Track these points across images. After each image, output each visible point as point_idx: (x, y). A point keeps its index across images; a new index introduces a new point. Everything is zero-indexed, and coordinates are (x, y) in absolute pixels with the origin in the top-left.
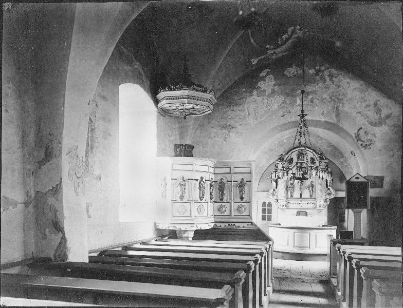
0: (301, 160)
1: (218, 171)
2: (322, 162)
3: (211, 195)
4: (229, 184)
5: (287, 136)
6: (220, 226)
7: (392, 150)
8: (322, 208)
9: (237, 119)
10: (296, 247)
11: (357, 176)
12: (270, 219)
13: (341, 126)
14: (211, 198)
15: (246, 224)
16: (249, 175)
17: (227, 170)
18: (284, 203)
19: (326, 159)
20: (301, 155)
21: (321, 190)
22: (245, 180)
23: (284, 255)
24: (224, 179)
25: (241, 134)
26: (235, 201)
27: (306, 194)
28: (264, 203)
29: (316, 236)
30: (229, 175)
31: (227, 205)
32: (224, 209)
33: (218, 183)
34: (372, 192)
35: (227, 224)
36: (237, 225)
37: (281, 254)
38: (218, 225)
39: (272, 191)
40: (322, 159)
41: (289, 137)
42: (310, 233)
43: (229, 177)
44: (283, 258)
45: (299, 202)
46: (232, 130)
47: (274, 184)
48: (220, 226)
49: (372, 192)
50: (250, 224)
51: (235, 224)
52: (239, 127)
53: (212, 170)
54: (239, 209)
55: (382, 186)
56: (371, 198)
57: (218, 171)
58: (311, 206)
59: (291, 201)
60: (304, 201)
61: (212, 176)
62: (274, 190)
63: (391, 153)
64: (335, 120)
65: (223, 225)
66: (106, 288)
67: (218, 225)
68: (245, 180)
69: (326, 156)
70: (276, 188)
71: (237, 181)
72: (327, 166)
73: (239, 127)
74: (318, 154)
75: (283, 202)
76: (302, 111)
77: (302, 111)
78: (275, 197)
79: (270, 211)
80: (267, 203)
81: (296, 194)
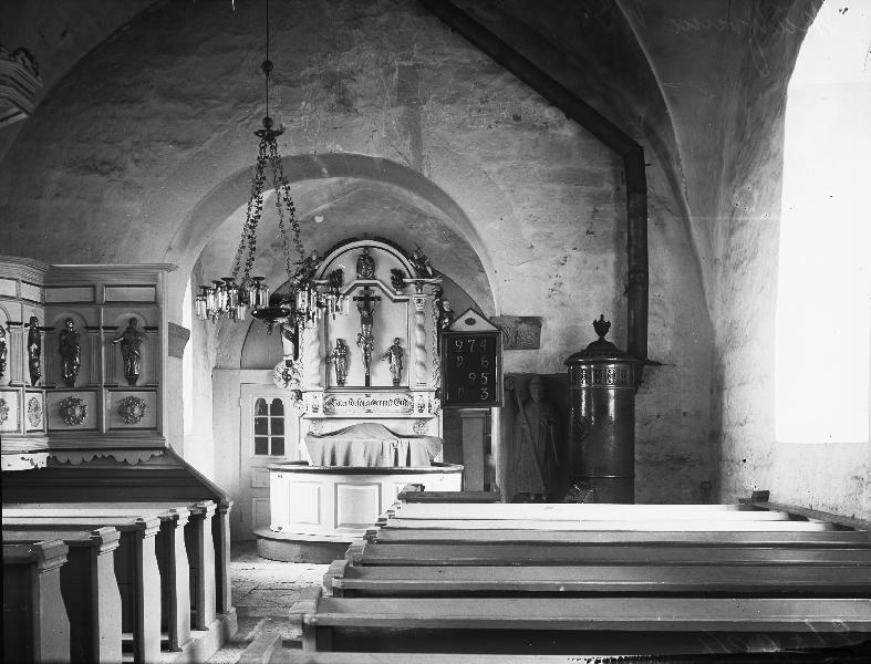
0: (366, 277)
1: (57, 295)
2: (423, 283)
3: (32, 368)
4: (93, 334)
5: (326, 206)
6: (68, 461)
7: (560, 247)
8: (425, 414)
9: (126, 143)
10: (342, 525)
11: (470, 314)
12: (279, 448)
13: (426, 175)
14: (35, 377)
15: (149, 453)
16: (152, 308)
17: (84, 294)
18: (320, 402)
19: (435, 274)
20: (366, 262)
21: (423, 365)
22: (141, 323)
23: (306, 549)
24: (76, 319)
25: (140, 188)
26: (112, 388)
27: (383, 374)
28: (261, 404)
29: (319, 489)
30: (91, 310)
31: (87, 398)
32: (78, 412)
33: (58, 331)
34: (512, 361)
35: (89, 457)
36: (120, 457)
37: (297, 548)
38: (62, 458)
39: (282, 366)
40: (423, 273)
41: (331, 209)
42: (380, 485)
43: (88, 312)
44: (304, 559)
45: (362, 397)
46: (114, 175)
47: (288, 346)
48: (68, 461)
49: (512, 361)
50: (157, 453)
51: (113, 454)
52: (131, 166)
53: (33, 293)
54: (123, 410)
55: (535, 345)
56: (509, 377)
57: (57, 295)
58: (397, 410)
59: (341, 397)
60: (375, 396)
61: (40, 313)
62: (289, 364)
63: (560, 255)
64: (411, 158)
65: (76, 459)
66: (783, 602)
67: (62, 458)
68: (141, 323)
69: (434, 266)
70: (296, 358)
71: (115, 328)
72: (439, 294)
73: (131, 166)
74: (413, 259)
75: (314, 399)
76: (268, 121)
77: (268, 121)
78: (293, 385)
79: (279, 427)
80: (269, 402)
81: (355, 376)
